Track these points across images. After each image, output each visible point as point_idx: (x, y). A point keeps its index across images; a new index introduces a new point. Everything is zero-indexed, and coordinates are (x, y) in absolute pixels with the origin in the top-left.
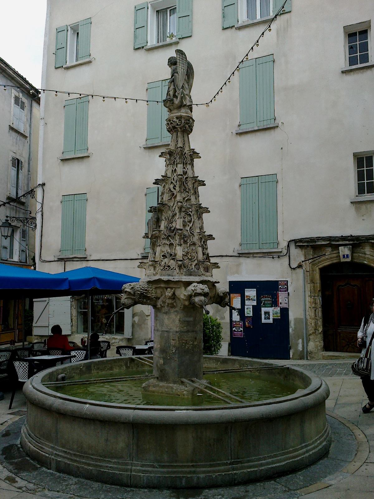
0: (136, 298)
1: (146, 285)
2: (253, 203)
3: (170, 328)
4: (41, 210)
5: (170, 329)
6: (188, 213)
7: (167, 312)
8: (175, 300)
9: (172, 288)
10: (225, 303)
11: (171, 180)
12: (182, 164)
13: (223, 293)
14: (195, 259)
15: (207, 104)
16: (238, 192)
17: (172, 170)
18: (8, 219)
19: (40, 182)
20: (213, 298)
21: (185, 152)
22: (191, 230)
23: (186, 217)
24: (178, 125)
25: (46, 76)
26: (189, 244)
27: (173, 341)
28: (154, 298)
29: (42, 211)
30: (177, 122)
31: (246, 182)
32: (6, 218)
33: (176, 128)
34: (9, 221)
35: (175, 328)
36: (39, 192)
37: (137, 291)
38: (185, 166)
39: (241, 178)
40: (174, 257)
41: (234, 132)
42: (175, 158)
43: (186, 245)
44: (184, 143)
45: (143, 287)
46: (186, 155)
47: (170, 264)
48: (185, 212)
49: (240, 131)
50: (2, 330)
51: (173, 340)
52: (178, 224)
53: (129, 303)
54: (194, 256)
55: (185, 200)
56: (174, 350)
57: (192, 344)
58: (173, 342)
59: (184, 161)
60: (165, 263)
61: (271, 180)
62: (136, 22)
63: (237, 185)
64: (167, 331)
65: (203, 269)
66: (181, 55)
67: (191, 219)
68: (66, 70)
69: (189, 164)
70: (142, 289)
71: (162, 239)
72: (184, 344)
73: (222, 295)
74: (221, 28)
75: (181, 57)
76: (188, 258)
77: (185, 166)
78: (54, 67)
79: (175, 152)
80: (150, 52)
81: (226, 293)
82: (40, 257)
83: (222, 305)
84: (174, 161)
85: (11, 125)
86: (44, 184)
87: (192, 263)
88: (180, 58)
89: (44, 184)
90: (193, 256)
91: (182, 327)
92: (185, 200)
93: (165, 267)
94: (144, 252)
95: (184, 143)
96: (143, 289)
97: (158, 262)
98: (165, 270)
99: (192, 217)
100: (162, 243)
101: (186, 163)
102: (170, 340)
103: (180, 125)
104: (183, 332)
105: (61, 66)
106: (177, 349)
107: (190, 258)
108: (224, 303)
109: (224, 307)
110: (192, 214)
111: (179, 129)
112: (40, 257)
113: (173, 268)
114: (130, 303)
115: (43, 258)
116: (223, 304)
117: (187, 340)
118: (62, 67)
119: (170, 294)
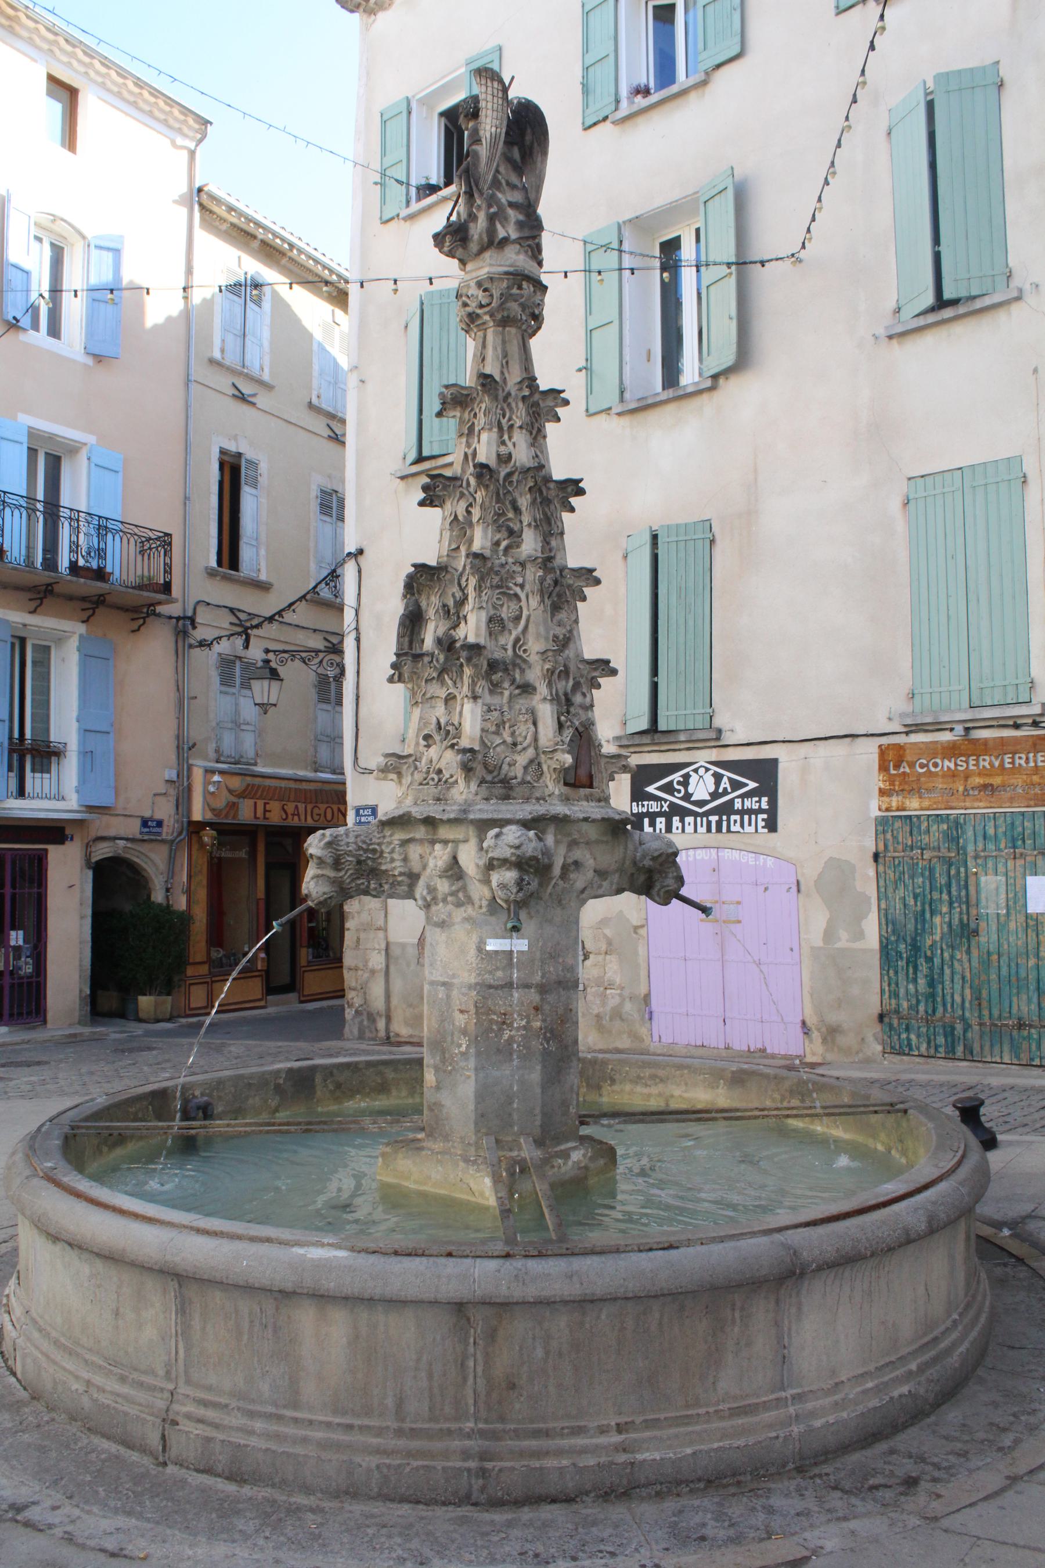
0: (346, 875)
1: (376, 834)
2: (949, 557)
3: (454, 974)
4: (353, 626)
5: (454, 976)
6: (512, 592)
7: (444, 922)
8: (460, 883)
9: (445, 842)
10: (667, 891)
11: (461, 486)
12: (495, 430)
13: (654, 859)
14: (525, 744)
15: (793, 255)
16: (900, 526)
17: (466, 455)
18: (271, 656)
19: (350, 547)
20: (617, 875)
21: (507, 390)
22: (520, 647)
23: (502, 606)
24: (481, 306)
25: (363, 249)
26: (507, 693)
27: (461, 1016)
28: (401, 874)
29: (357, 629)
30: (480, 298)
31: (923, 492)
32: (264, 656)
33: (478, 316)
34: (273, 665)
35: (466, 974)
36: (349, 571)
37: (349, 853)
38: (506, 437)
39: (909, 479)
40: (455, 741)
41: (881, 332)
42: (475, 415)
43: (499, 697)
44: (507, 363)
45: (364, 842)
46: (510, 400)
47: (442, 765)
48: (498, 587)
49: (900, 329)
50: (309, 962)
51: (462, 1012)
52: (472, 628)
53: (321, 893)
54: (524, 734)
55: (502, 547)
56: (464, 1046)
57: (525, 1028)
58: (460, 1020)
59: (504, 422)
60: (431, 761)
61: (1008, 478)
62: (586, 50)
63: (895, 504)
64: (444, 984)
65: (554, 777)
66: (489, 84)
67: (521, 612)
68: (408, 223)
69: (521, 427)
70: (362, 848)
71: (427, 681)
72: (494, 1027)
73: (647, 863)
74: (833, 11)
75: (490, 89)
76: (504, 742)
77: (506, 437)
78: (379, 222)
79: (475, 395)
80: (628, 124)
81: (663, 857)
82: (356, 758)
83: (657, 899)
84: (473, 424)
85: (315, 401)
86: (361, 552)
87: (517, 757)
88: (486, 93)
89: (361, 552)
90: (520, 735)
91: (490, 972)
92: (502, 547)
93: (428, 773)
94: (623, 734)
95: (507, 363)
96: (364, 846)
97: (411, 760)
98: (428, 784)
99: (523, 603)
100: (424, 695)
101: (511, 427)
102: (453, 1011)
103: (488, 305)
104: (490, 987)
105: (394, 214)
106: (475, 1041)
107: (509, 740)
108: (659, 890)
109: (666, 903)
110: (523, 596)
111: (487, 318)
112: (356, 758)
113: (452, 776)
114: (324, 893)
115: (362, 763)
116: (658, 895)
117: (505, 1014)
118: (398, 215)
119: (441, 864)
